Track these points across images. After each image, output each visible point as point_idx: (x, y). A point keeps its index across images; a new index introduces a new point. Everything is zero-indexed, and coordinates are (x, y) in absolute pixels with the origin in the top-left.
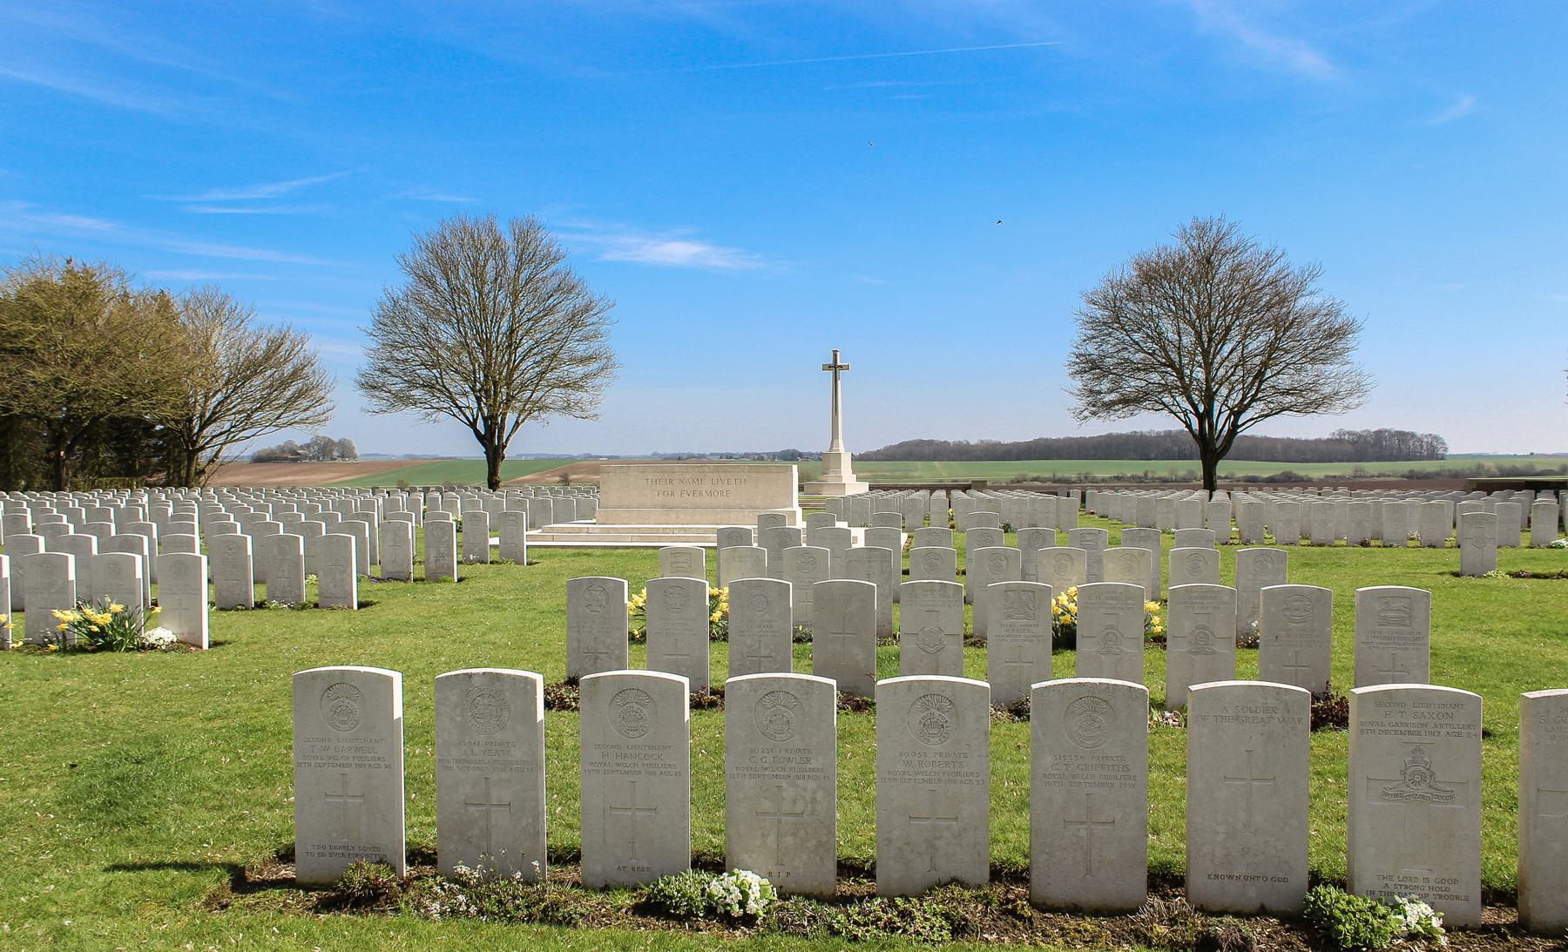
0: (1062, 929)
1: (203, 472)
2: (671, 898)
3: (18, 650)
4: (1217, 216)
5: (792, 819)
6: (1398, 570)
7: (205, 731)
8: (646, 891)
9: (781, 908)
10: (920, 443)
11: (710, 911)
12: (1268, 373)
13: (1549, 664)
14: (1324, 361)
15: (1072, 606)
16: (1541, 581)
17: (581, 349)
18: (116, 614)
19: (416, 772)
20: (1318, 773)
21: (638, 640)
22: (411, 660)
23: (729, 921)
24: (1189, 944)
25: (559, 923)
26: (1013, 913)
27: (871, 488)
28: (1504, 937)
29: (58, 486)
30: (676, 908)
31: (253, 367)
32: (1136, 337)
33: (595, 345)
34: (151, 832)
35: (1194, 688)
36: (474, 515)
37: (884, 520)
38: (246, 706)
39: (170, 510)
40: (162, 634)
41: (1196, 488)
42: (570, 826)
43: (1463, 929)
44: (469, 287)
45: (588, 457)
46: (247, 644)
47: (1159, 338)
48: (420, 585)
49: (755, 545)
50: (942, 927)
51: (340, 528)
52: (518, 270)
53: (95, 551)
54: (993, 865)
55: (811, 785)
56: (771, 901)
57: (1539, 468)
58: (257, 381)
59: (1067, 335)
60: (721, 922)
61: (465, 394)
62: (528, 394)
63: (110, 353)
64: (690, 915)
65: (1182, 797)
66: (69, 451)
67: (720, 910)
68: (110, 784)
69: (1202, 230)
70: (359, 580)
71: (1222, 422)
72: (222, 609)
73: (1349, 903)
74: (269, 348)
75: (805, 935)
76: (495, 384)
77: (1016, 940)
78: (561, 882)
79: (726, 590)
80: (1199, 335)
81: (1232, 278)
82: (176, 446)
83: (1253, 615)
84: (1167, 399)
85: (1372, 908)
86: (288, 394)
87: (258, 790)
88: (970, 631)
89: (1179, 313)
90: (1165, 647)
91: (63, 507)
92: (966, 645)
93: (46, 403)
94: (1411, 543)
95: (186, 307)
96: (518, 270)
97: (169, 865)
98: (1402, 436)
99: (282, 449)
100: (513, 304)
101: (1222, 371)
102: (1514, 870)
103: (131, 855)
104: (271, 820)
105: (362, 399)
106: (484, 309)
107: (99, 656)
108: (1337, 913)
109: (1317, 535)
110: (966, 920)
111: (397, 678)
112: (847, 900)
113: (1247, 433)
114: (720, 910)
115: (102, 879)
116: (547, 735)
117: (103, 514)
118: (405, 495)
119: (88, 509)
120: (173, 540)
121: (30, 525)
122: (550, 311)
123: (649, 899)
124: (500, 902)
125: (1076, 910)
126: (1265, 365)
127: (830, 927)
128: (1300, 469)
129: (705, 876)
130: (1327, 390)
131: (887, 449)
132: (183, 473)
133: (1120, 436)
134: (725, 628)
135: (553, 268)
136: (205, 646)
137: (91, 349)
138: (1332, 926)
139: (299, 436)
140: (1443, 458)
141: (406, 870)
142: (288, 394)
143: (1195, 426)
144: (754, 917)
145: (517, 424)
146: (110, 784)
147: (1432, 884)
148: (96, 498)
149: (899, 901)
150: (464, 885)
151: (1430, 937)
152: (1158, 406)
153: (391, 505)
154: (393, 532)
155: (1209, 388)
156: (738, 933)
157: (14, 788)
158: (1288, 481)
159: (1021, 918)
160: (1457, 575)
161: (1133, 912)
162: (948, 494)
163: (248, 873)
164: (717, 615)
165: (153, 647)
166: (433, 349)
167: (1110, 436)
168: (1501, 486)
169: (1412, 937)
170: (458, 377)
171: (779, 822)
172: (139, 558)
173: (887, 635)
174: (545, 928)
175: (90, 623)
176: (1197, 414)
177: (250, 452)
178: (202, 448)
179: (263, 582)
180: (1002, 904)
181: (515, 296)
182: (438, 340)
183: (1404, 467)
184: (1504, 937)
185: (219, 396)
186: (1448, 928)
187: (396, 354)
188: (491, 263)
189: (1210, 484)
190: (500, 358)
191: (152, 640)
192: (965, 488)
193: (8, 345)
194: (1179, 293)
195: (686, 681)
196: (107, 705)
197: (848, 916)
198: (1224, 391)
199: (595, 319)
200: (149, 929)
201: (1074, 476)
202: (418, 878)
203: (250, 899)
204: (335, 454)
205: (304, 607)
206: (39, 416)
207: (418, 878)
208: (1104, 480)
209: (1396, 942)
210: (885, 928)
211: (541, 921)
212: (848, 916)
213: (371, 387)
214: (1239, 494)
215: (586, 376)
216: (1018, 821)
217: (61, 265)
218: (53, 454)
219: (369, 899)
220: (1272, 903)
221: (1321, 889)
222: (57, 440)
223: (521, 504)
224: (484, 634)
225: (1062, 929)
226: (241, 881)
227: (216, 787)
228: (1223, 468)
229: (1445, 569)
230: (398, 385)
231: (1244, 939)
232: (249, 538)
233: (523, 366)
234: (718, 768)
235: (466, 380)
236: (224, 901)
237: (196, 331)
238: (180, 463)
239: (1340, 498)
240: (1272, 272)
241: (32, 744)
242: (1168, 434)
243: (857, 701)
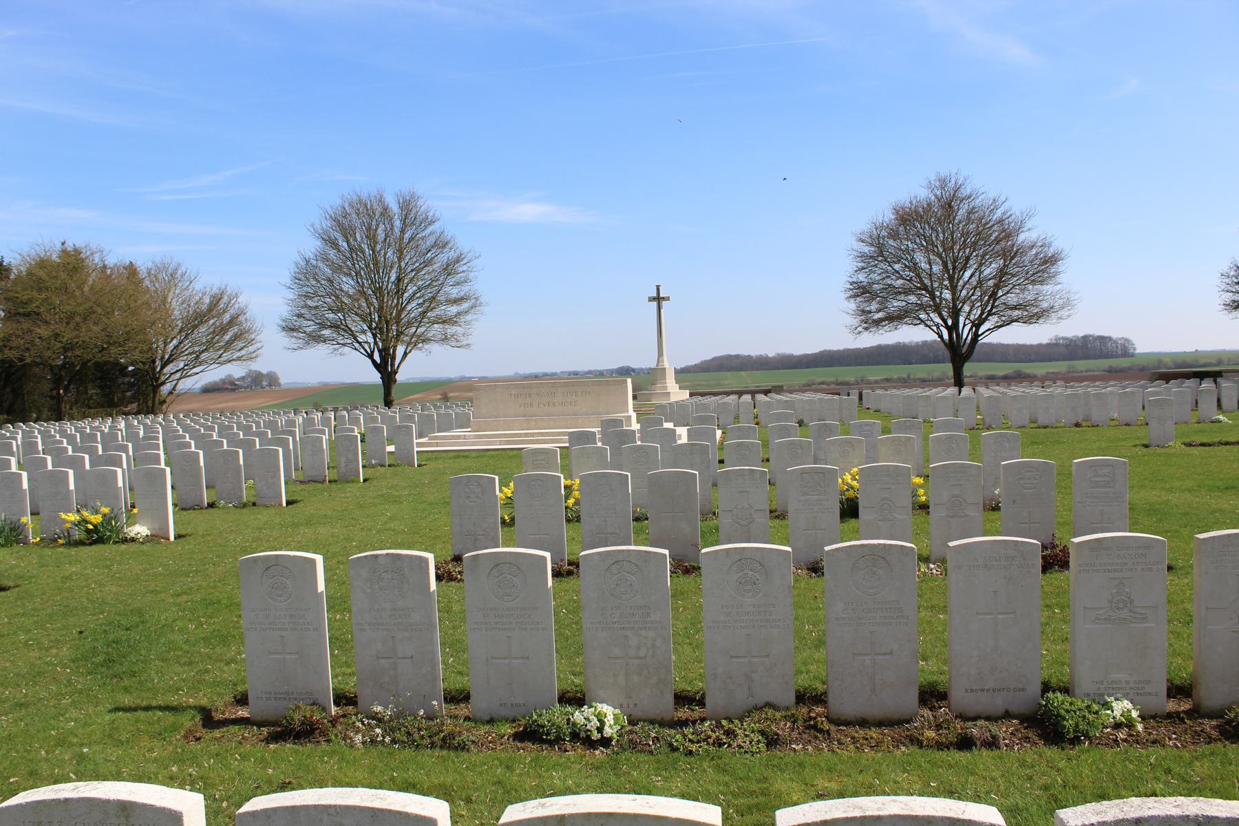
0: (853, 738)
1: (164, 402)
2: (543, 727)
3: (36, 544)
4: (954, 171)
5: (637, 661)
6: (1103, 444)
7: (175, 604)
8: (523, 722)
9: (631, 732)
10: (729, 357)
11: (575, 736)
12: (1000, 293)
13: (1214, 512)
14: (1042, 283)
15: (855, 483)
16: (1207, 448)
17: (454, 292)
18: (105, 515)
19: (337, 634)
20: (1047, 606)
21: (508, 524)
22: (329, 545)
23: (589, 743)
24: (951, 743)
25: (456, 749)
26: (815, 727)
27: (691, 395)
28: (1182, 720)
29: (59, 418)
30: (548, 734)
31: (199, 318)
32: (897, 267)
33: (464, 290)
34: (141, 682)
35: (951, 544)
36: (375, 428)
37: (703, 420)
38: (205, 584)
39: (141, 433)
40: (140, 530)
41: (948, 386)
42: (460, 673)
43: (1154, 717)
44: (365, 247)
45: (463, 379)
46: (203, 536)
47: (914, 267)
48: (334, 486)
49: (599, 444)
50: (759, 742)
51: (270, 442)
52: (403, 231)
53: (88, 467)
54: (798, 691)
55: (651, 634)
56: (623, 727)
57: (1202, 361)
58: (203, 329)
59: (842, 268)
60: (583, 744)
61: (364, 332)
62: (413, 329)
63: (94, 312)
64: (559, 739)
65: (945, 630)
66: (66, 389)
67: (583, 735)
68: (108, 646)
69: (943, 183)
70: (286, 483)
72: (183, 509)
73: (1071, 704)
74: (211, 302)
75: (651, 752)
76: (387, 322)
77: (817, 749)
78: (456, 717)
79: (578, 481)
80: (945, 264)
81: (968, 218)
82: (144, 382)
83: (996, 485)
84: (923, 316)
85: (1088, 707)
86: (227, 337)
87: (218, 650)
88: (773, 507)
89: (929, 248)
90: (928, 513)
91: (63, 433)
92: (771, 518)
93: (48, 353)
94: (1113, 423)
95: (149, 273)
96: (403, 231)
97: (155, 708)
98: (1102, 339)
99: (223, 381)
100: (400, 259)
101: (964, 293)
102: (1190, 669)
103: (127, 700)
104: (229, 673)
105: (283, 340)
106: (376, 264)
107: (94, 548)
108: (1063, 712)
109: (1042, 420)
110: (777, 734)
111: (319, 559)
112: (683, 723)
113: (985, 341)
114: (583, 735)
115: (107, 718)
116: (439, 602)
117: (92, 437)
118: (320, 414)
119: (82, 433)
120: (143, 458)
121: (40, 448)
122: (428, 263)
123: (525, 728)
124: (408, 733)
125: (864, 723)
126: (997, 286)
127: (671, 745)
128: (1027, 368)
129: (569, 709)
130: (1045, 305)
132: (150, 403)
133: (887, 346)
134: (578, 511)
135: (430, 229)
136: (172, 538)
137: (80, 310)
138: (1058, 722)
139: (236, 371)
140: (1133, 355)
141: (334, 710)
142: (227, 337)
143: (946, 336)
144: (610, 739)
145: (405, 354)
146: (108, 646)
147: (1132, 685)
148: (87, 425)
149: (724, 722)
150: (380, 720)
151: (1130, 725)
153: (308, 423)
154: (309, 443)
155: (955, 305)
156: (597, 752)
157: (40, 649)
158: (1019, 378)
159: (821, 731)
160: (1146, 446)
161: (908, 722)
162: (753, 398)
163: (213, 714)
164: (571, 501)
165: (133, 540)
166: (337, 297)
167: (879, 347)
168: (1176, 376)
169: (1118, 726)
170: (357, 319)
171: (627, 664)
172: (119, 471)
173: (709, 513)
174: (445, 752)
175: (87, 522)
176: (947, 327)
177: (199, 386)
178: (164, 383)
179: (213, 487)
180: (805, 721)
181: (400, 253)
182: (341, 290)
183: (1105, 363)
184: (1182, 720)
185: (175, 342)
186: (1143, 717)
187: (309, 303)
188: (382, 227)
189: (959, 382)
190: (390, 302)
191: (132, 534)
192: (766, 392)
193: (21, 310)
194: (928, 232)
195: (547, 555)
196: (102, 585)
197: (684, 736)
198: (967, 308)
199: (465, 268)
200: (144, 755)
201: (852, 379)
202: (344, 716)
203: (217, 733)
204: (265, 383)
205: (245, 506)
206: (44, 364)
207: (344, 716)
208: (876, 382)
209: (1106, 731)
210: (714, 744)
211: (442, 747)
212: (684, 736)
213: (290, 329)
214: (981, 389)
215: (459, 314)
216: (817, 656)
217: (59, 246)
218: (54, 392)
219: (305, 732)
220: (1014, 709)
221: (1050, 695)
222: (57, 381)
223: (411, 418)
224: (386, 523)
225: (853, 738)
226: (209, 721)
227: (186, 647)
228: (969, 369)
229: (1138, 442)
230: (311, 327)
231: (993, 737)
232: (201, 453)
233: (409, 308)
234: (576, 623)
235: (364, 321)
236: (198, 735)
237: (156, 292)
238: (148, 395)
239: (1058, 389)
241: (51, 616)
242: (925, 343)
243: (686, 567)
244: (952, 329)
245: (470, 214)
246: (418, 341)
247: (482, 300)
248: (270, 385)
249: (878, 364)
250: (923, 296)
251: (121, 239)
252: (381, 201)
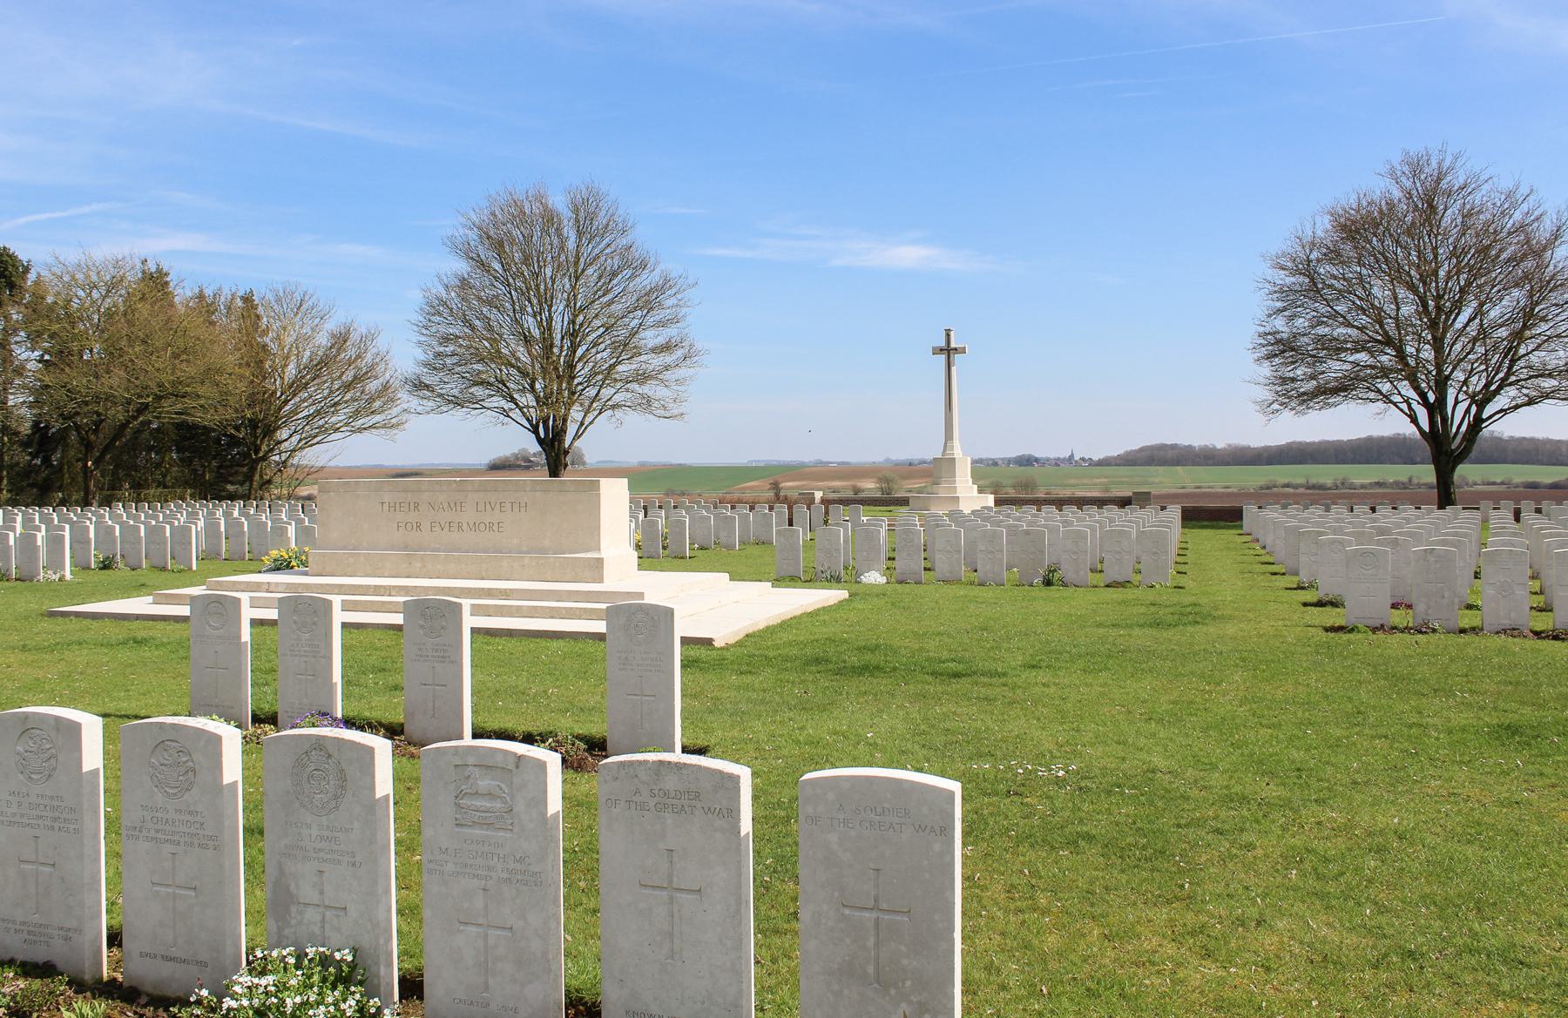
10: (1163, 447)
12: (1522, 351)
27: (998, 502)
33: (671, 332)
61: (523, 391)
66: (97, 462)
69: (1416, 169)
71: (1459, 414)
84: (1385, 387)
89: (1397, 275)
99: (516, 456)
131: (1128, 453)
133: (1382, 439)
152: (1372, 395)
167: (1370, 439)
198: (1459, 375)
228: (1467, 473)
240: (1517, 216)
244: (1436, 409)
245: (667, 222)
246: (600, 407)
247: (698, 346)
249: (1368, 462)
250: (1385, 359)
251: (206, 255)
252: (540, 198)
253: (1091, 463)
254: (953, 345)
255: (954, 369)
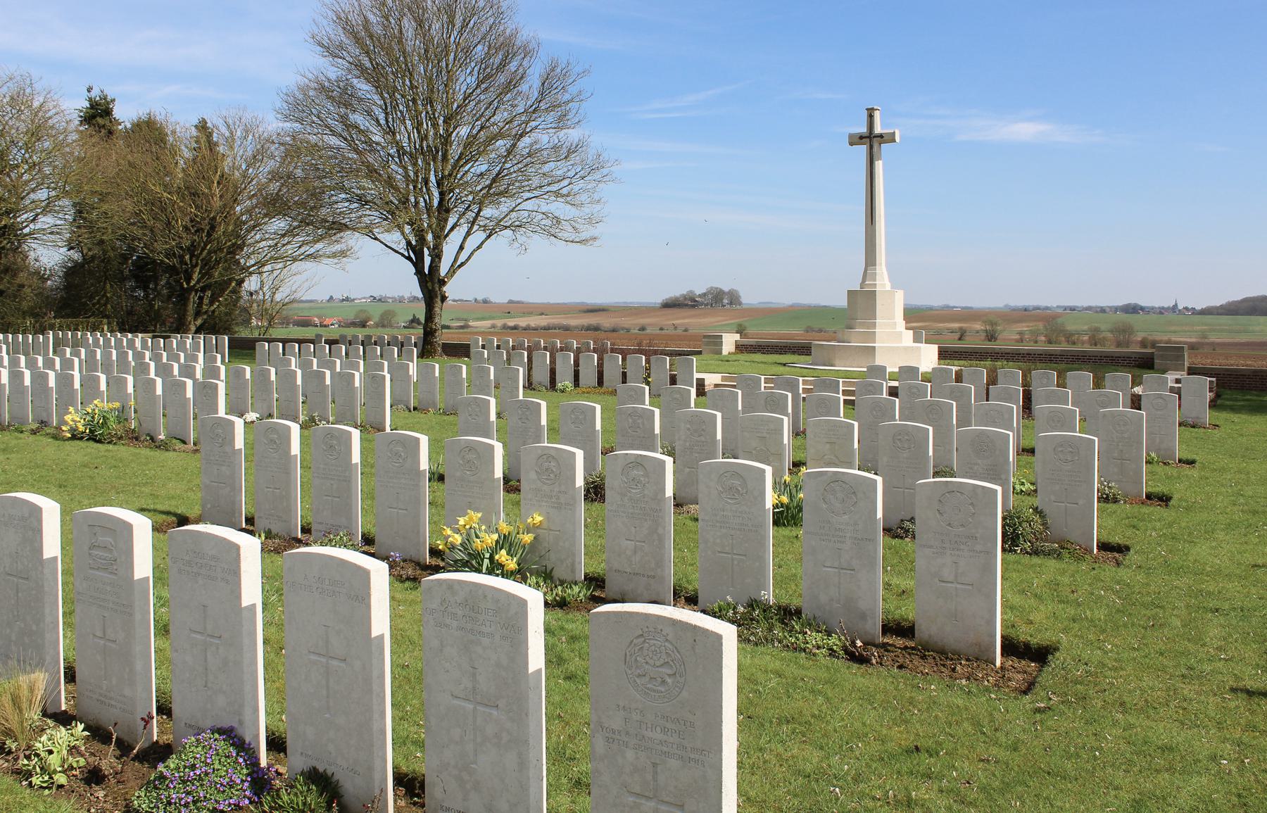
27: (944, 354)
99: (685, 297)
131: (1230, 304)
204: (726, 301)
248: (731, 303)
253: (1194, 312)
254: (878, 129)
255: (879, 165)
